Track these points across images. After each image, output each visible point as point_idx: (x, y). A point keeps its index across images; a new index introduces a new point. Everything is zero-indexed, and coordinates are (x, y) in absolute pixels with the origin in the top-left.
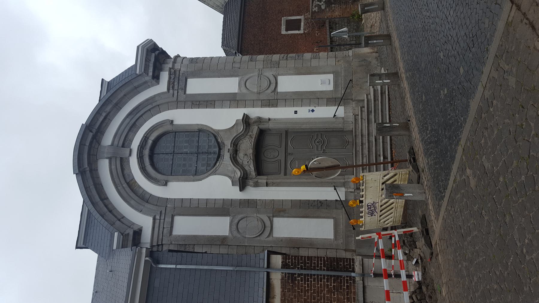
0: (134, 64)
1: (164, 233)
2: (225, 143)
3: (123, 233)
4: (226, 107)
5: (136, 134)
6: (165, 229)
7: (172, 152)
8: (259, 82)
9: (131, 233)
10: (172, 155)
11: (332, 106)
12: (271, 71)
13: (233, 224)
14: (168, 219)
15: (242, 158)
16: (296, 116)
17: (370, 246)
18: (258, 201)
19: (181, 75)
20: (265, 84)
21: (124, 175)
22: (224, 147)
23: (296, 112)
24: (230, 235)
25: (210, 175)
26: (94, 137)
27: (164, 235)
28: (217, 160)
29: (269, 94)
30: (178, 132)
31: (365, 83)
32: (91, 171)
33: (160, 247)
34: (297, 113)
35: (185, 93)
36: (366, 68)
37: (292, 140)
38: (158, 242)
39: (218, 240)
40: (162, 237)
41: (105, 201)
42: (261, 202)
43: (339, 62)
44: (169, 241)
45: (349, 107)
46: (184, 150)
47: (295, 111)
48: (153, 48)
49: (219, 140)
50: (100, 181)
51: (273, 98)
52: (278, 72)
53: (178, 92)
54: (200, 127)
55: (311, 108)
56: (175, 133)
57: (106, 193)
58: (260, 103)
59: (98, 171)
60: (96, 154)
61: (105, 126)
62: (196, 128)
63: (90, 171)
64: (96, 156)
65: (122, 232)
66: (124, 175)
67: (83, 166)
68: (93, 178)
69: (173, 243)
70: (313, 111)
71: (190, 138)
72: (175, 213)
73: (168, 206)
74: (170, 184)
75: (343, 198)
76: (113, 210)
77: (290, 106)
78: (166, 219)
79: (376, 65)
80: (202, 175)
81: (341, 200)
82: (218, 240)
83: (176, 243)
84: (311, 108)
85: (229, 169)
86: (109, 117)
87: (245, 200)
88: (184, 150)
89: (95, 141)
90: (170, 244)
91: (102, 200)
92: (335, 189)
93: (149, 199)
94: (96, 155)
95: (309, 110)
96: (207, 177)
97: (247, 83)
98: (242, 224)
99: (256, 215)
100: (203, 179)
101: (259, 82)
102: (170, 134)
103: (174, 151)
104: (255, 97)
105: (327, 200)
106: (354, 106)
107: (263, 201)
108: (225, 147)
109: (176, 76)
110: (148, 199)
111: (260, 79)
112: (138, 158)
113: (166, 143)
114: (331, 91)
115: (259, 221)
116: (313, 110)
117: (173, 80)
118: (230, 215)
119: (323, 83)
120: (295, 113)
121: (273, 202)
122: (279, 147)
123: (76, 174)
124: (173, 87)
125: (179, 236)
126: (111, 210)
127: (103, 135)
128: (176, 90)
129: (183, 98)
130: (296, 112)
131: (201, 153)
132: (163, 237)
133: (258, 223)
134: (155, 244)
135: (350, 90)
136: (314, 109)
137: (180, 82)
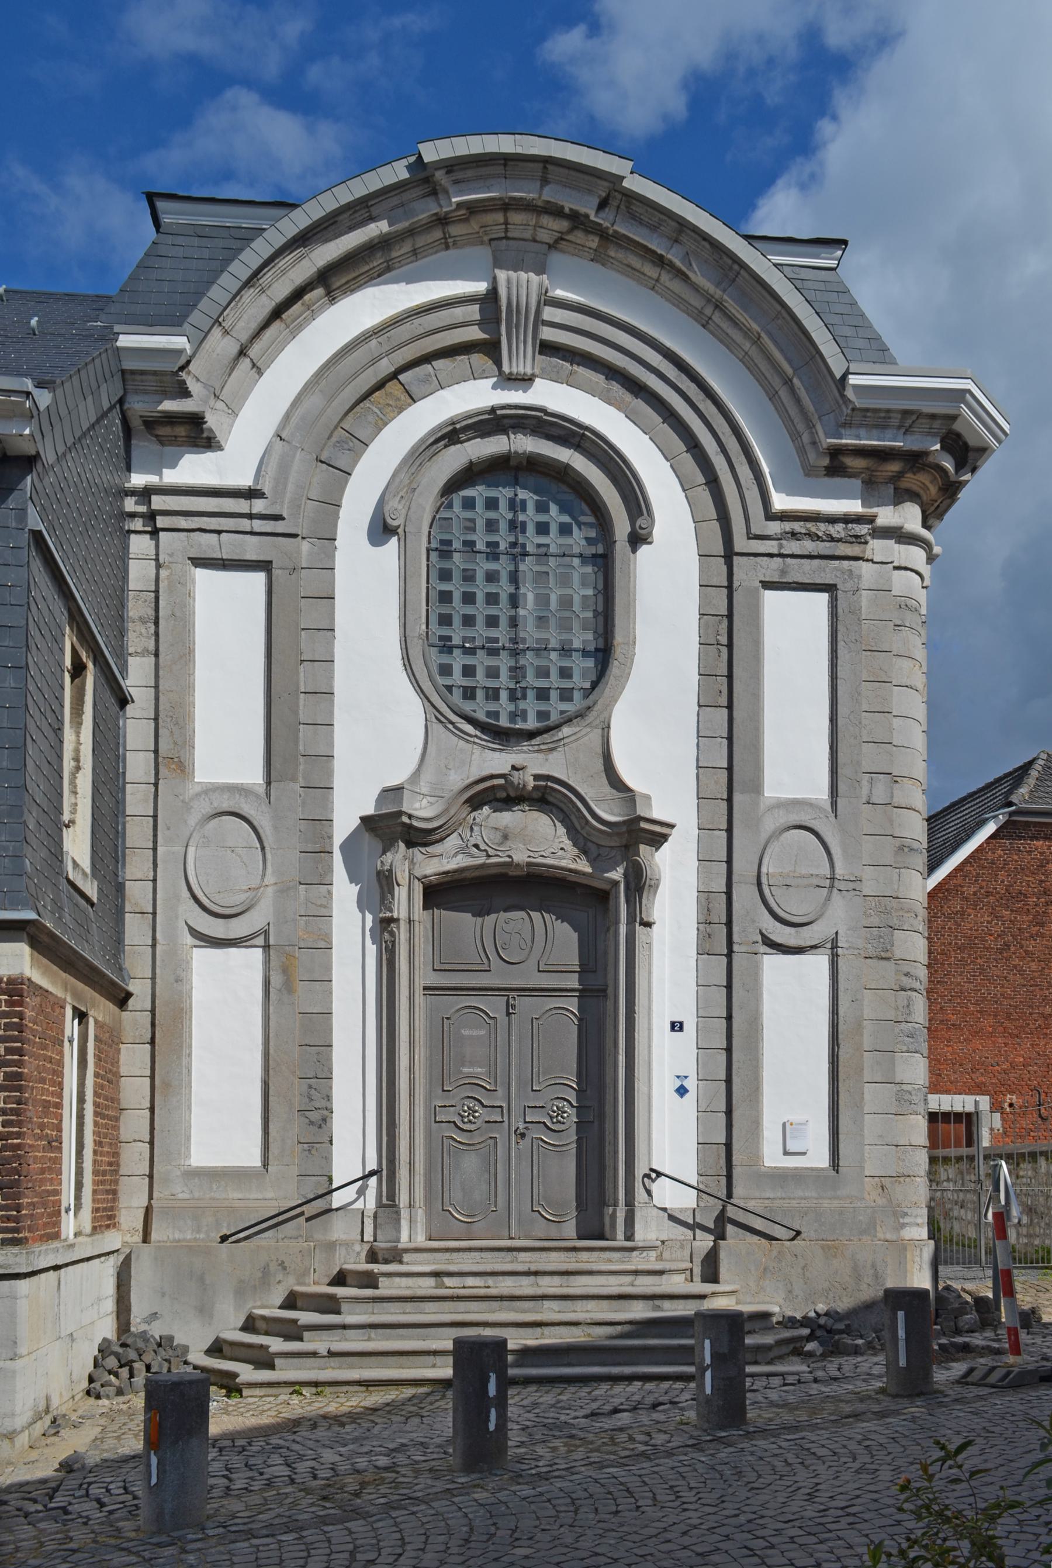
8: (805, 882)
13: (237, 796)
16: (660, 1025)
17: (163, 1295)
23: (677, 1026)
29: (754, 921)
32: (442, 221)
34: (681, 1023)
39: (175, 743)
42: (323, 902)
44: (171, 555)
46: (530, 597)
49: (566, 730)
55: (691, 1084)
60: (510, 235)
64: (503, 235)
67: (456, 182)
70: (682, 1091)
81: (334, 1194)
84: (691, 1084)
85: (452, 772)
87: (327, 841)
88: (530, 597)
89: (564, 225)
94: (507, 238)
95: (686, 1077)
101: (805, 882)
107: (325, 907)
121: (322, 944)
125: (190, 595)
129: (745, 577)
136: (691, 1097)
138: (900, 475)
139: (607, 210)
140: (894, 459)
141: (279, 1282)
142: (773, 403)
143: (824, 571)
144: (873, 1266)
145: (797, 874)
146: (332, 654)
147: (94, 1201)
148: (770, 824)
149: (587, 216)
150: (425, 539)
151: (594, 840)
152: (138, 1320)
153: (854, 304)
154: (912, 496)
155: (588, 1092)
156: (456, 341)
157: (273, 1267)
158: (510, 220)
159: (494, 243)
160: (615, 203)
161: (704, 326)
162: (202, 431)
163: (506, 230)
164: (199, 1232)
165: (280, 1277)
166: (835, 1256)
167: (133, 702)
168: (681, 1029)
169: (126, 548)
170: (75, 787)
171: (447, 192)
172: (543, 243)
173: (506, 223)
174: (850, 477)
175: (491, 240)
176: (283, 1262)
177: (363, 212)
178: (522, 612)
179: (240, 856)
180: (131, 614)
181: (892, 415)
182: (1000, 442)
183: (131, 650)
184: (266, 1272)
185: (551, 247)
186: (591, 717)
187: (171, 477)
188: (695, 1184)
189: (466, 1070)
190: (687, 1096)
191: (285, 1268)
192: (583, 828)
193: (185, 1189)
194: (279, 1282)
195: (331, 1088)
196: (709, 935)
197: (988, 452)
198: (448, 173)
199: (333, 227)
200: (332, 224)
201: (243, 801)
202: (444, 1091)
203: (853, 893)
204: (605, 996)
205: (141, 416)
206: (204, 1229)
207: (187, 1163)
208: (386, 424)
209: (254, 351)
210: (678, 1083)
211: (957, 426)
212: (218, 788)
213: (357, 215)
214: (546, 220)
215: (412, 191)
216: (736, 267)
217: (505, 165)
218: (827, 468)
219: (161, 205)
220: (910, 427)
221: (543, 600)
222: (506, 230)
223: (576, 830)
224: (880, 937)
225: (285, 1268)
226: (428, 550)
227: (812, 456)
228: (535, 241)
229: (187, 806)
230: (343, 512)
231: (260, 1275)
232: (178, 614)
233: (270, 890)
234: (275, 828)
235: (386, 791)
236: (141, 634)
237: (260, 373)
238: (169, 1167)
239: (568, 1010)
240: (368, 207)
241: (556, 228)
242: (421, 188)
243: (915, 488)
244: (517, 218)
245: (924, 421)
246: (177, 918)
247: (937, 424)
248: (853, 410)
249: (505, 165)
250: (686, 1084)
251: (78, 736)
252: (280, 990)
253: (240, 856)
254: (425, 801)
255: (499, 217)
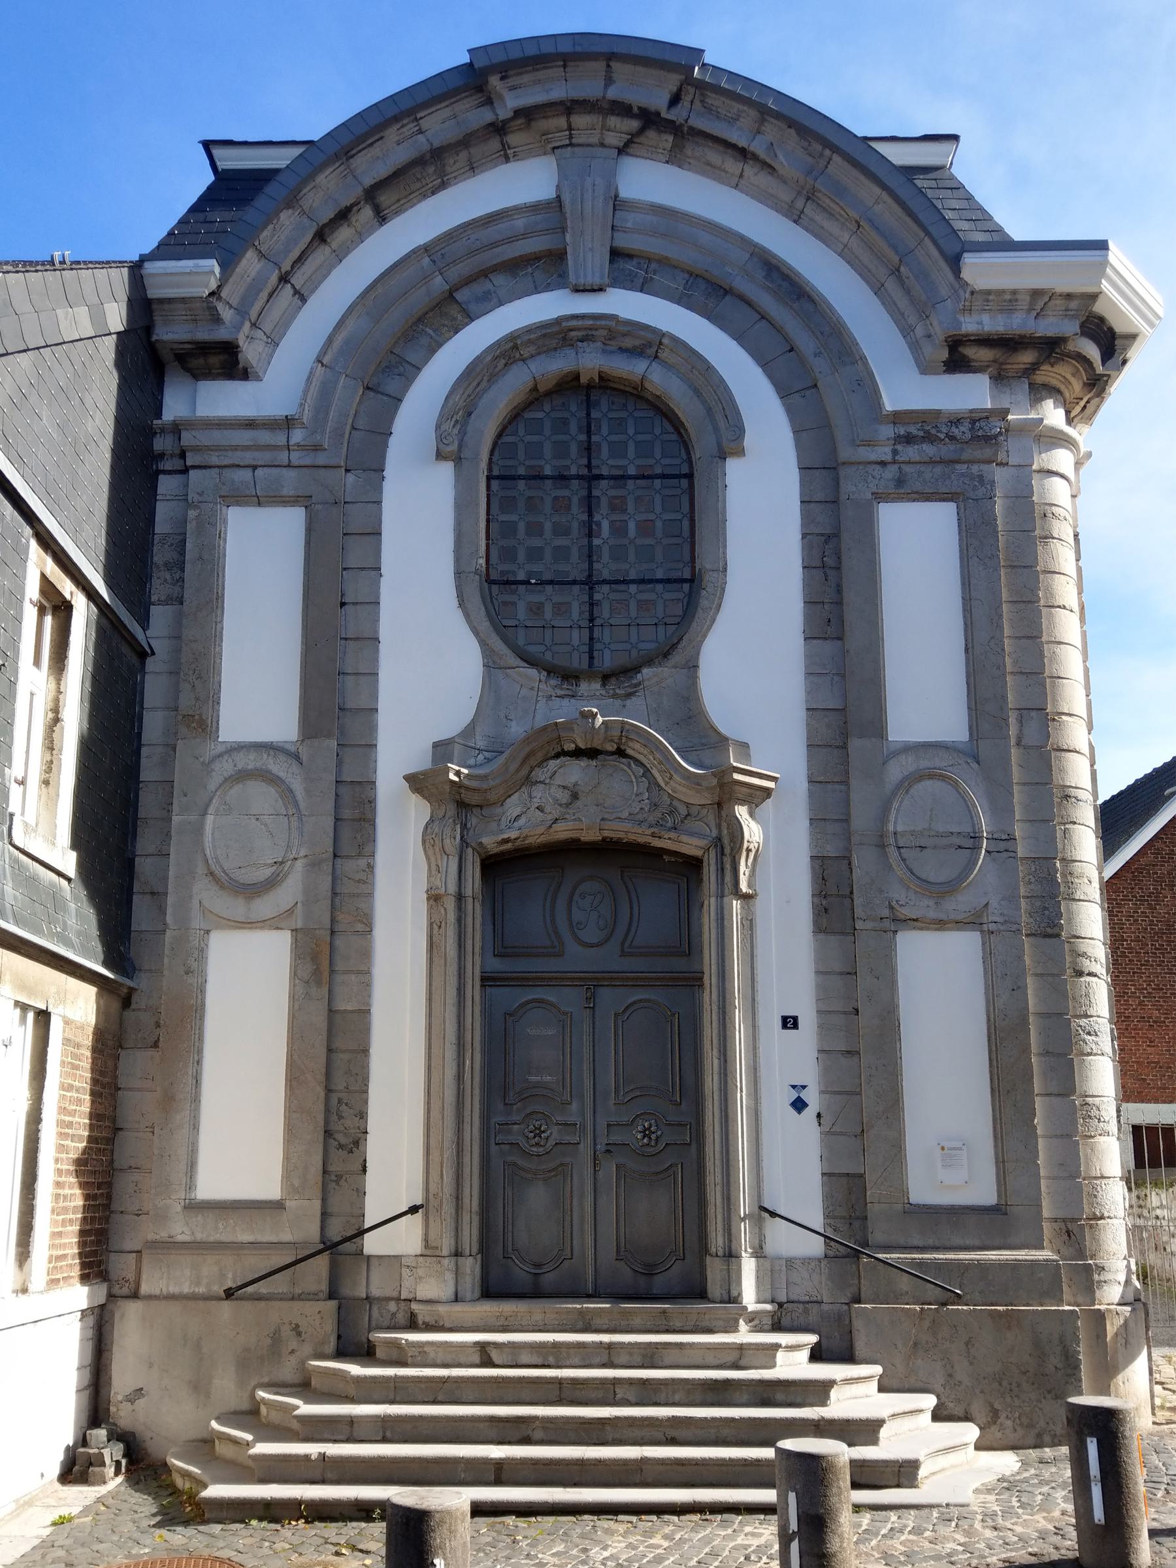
0: (1016, 239)
1: (236, 470)
2: (634, 698)
3: (220, 298)
4: (810, 692)
5: (678, 303)
6: (246, 474)
7: (595, 472)
8: (945, 841)
9: (222, 334)
10: (585, 472)
11: (828, 1197)
12: (1003, 899)
13: (265, 756)
14: (290, 481)
15: (558, 780)
17: (151, 1366)
18: (362, 862)
19: (975, 469)
20: (935, 869)
21: (485, 273)
22: (615, 696)
23: (790, 1022)
24: (220, 749)
25: (483, 643)
26: (649, 119)
27: (226, 472)
28: (551, 671)
29: (881, 891)
30: (691, 486)
31: (945, 1366)
32: (499, 129)
33: (177, 464)
34: (795, 1019)
35: (880, 497)
36: (1025, 1373)
37: (646, 1004)
38: (196, 449)
39: (197, 699)
40: (219, 467)
41: (367, 212)
42: (362, 876)
43: (1066, 1237)
44: (201, 494)
45: (821, 1283)
46: (605, 525)
47: (795, 1019)
48: (1111, 330)
50: (457, 179)
51: (858, 912)
52: (999, 931)
53: (883, 464)
54: (709, 578)
55: (812, 1097)
56: (685, 476)
57: (407, 210)
58: (831, 851)
59: (504, 166)
60: (574, 141)
61: (708, 164)
62: (705, 561)
63: (492, 124)
64: (567, 142)
65: (224, 294)
66: (485, 273)
67: (513, 88)
68: (465, 142)
69: (192, 514)
70: (799, 1105)
71: (665, 541)
72: (320, 507)
73: (351, 478)
74: (447, 470)
75: (372, 1244)
76: (327, 248)
77: (823, 995)
78: (291, 474)
79: (1042, 1424)
80: (483, 609)
81: (366, 1236)
82: (197, 699)
83: (191, 527)
84: (812, 1097)
85: (514, 724)
86: (750, 170)
88: (605, 525)
89: (635, 124)
90: (187, 500)
91: (371, 194)
92: (413, 1210)
93: (380, 396)
94: (571, 145)
95: (804, 1087)
96: (476, 632)
97: (928, 783)
98: (261, 797)
99: (302, 853)
100: (467, 616)
101: (945, 841)
102: (683, 451)
103: (600, 477)
104: (862, 819)
105: (364, 1170)
106: (825, 1307)
107: (365, 882)
108: (618, 702)
109: (965, 446)
110: (380, 390)
111: (960, 847)
112: (559, 321)
113: (640, 437)
114: (905, 1192)
115: (275, 868)
116: (805, 1105)
117: (942, 436)
118: (303, 741)
119: (949, 1153)
120: (795, 1026)
121: (360, 927)
122: (626, 945)
123: (471, 64)
124: (908, 439)
125: (222, 536)
126: (328, 240)
127: (667, 162)
128: (895, 452)
129: (854, 489)
130: (790, 1022)
131: (591, 597)
132: (217, 470)
133: (265, 865)
134: (187, 439)
135: (905, 1288)
137: (938, 469)
138: (1034, 368)
139: (680, 105)
140: (1026, 349)
141: (293, 1352)
142: (878, 297)
143: (949, 478)
144: (1062, 1340)
145: (932, 833)
146: (378, 597)
147: (53, 1246)
148: (895, 771)
149: (658, 114)
150: (484, 465)
151: (682, 798)
152: (120, 1398)
153: (969, 198)
154: (1053, 391)
155: (683, 1105)
156: (517, 254)
157: (286, 1331)
158: (573, 125)
159: (557, 151)
160: (689, 98)
161: (795, 222)
162: (237, 362)
163: (571, 137)
164: (198, 1284)
165: (293, 1344)
166: (1009, 1328)
167: (153, 653)
168: (795, 1026)
169: (154, 488)
170: (52, 741)
171: (501, 98)
172: (610, 147)
173: (570, 128)
174: (975, 372)
175: (554, 148)
176: (297, 1326)
177: (412, 125)
178: (596, 542)
179: (266, 825)
180: (155, 559)
181: (1018, 297)
182: (1152, 325)
183: (154, 598)
184: (276, 1338)
185: (622, 151)
186: (677, 658)
187: (205, 410)
188: (822, 1231)
189: (533, 1078)
190: (806, 1111)
191: (299, 1334)
192: (667, 784)
193: (185, 1229)
194: (293, 1352)
195: (366, 1102)
196: (826, 910)
197: (1139, 339)
198: (502, 79)
199: (380, 142)
200: (378, 140)
201: (271, 761)
202: (506, 1104)
203: (1005, 855)
204: (701, 986)
205: (172, 349)
206: (205, 1281)
207: (193, 1197)
208: (440, 345)
209: (298, 279)
210: (794, 1095)
211: (1099, 308)
212: (243, 747)
213: (404, 130)
214: (613, 121)
215: (465, 101)
216: (827, 152)
217: (565, 66)
218: (946, 363)
219: (217, 152)
220: (1042, 309)
221: (619, 530)
222: (571, 137)
223: (659, 786)
224: (1045, 908)
225: (299, 1334)
226: (489, 478)
227: (928, 350)
228: (602, 145)
229: (207, 766)
230: (393, 441)
231: (269, 1341)
232: (205, 557)
233: (299, 864)
234: (308, 791)
235: (436, 745)
236: (165, 580)
237: (304, 300)
238: (169, 1201)
239: (635, 1003)
240: (416, 120)
241: (624, 129)
242: (474, 97)
243: (1055, 382)
244: (581, 120)
245: (1058, 302)
246: (191, 897)
247: (1074, 304)
248: (972, 293)
249: (565, 66)
250: (804, 1095)
251: (59, 684)
252: (307, 982)
253: (266, 825)
254: (481, 757)
255: (562, 122)
